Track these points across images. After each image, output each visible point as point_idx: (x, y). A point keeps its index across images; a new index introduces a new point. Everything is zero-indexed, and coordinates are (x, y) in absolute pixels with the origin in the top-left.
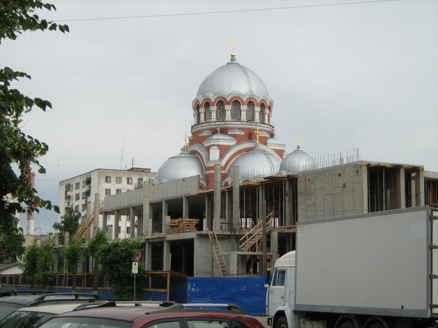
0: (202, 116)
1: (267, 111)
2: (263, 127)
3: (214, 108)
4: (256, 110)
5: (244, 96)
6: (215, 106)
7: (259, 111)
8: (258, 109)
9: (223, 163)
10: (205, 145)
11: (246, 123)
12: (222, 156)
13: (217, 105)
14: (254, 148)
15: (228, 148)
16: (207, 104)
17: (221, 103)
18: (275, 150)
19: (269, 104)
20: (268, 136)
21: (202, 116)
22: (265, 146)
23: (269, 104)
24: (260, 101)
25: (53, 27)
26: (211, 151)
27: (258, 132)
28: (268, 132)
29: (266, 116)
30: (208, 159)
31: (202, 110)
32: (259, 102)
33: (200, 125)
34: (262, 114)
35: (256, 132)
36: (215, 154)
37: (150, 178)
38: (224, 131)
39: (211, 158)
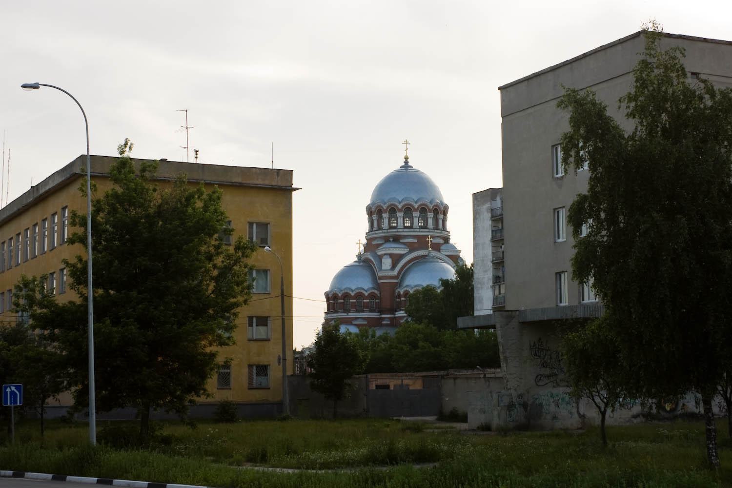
0: (375, 223)
1: (441, 216)
2: (436, 232)
3: (385, 215)
4: (440, 217)
5: (400, 203)
6: (388, 214)
7: (432, 217)
8: (430, 215)
9: (395, 272)
10: (379, 253)
11: (418, 230)
12: (394, 267)
13: (377, 214)
14: (427, 256)
15: (401, 256)
16: (380, 212)
17: (423, 210)
18: (449, 256)
19: (442, 209)
20: (442, 241)
21: (375, 223)
22: (438, 253)
23: (442, 209)
24: (433, 207)
25: (196, 154)
26: (383, 260)
27: (430, 239)
28: (441, 238)
29: (440, 222)
30: (381, 269)
31: (375, 217)
32: (432, 207)
33: (373, 233)
34: (436, 220)
35: (427, 239)
36: (387, 263)
37: (498, 326)
38: (396, 239)
39: (384, 267)
